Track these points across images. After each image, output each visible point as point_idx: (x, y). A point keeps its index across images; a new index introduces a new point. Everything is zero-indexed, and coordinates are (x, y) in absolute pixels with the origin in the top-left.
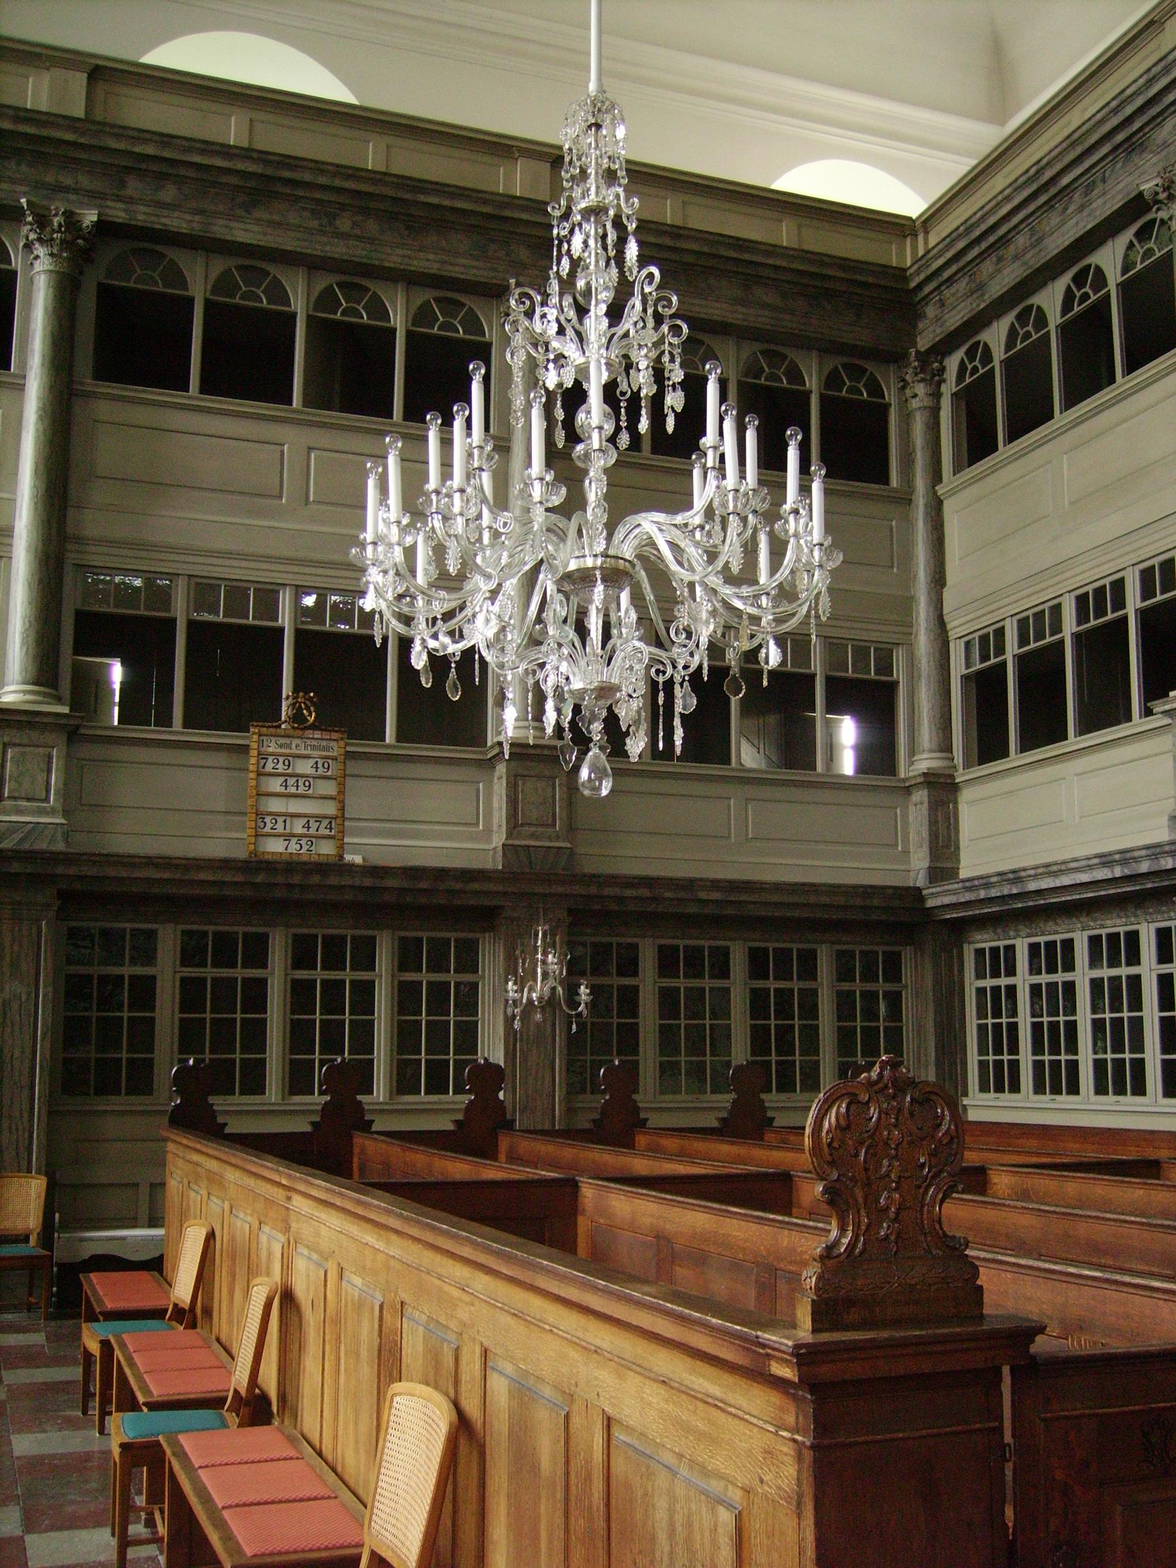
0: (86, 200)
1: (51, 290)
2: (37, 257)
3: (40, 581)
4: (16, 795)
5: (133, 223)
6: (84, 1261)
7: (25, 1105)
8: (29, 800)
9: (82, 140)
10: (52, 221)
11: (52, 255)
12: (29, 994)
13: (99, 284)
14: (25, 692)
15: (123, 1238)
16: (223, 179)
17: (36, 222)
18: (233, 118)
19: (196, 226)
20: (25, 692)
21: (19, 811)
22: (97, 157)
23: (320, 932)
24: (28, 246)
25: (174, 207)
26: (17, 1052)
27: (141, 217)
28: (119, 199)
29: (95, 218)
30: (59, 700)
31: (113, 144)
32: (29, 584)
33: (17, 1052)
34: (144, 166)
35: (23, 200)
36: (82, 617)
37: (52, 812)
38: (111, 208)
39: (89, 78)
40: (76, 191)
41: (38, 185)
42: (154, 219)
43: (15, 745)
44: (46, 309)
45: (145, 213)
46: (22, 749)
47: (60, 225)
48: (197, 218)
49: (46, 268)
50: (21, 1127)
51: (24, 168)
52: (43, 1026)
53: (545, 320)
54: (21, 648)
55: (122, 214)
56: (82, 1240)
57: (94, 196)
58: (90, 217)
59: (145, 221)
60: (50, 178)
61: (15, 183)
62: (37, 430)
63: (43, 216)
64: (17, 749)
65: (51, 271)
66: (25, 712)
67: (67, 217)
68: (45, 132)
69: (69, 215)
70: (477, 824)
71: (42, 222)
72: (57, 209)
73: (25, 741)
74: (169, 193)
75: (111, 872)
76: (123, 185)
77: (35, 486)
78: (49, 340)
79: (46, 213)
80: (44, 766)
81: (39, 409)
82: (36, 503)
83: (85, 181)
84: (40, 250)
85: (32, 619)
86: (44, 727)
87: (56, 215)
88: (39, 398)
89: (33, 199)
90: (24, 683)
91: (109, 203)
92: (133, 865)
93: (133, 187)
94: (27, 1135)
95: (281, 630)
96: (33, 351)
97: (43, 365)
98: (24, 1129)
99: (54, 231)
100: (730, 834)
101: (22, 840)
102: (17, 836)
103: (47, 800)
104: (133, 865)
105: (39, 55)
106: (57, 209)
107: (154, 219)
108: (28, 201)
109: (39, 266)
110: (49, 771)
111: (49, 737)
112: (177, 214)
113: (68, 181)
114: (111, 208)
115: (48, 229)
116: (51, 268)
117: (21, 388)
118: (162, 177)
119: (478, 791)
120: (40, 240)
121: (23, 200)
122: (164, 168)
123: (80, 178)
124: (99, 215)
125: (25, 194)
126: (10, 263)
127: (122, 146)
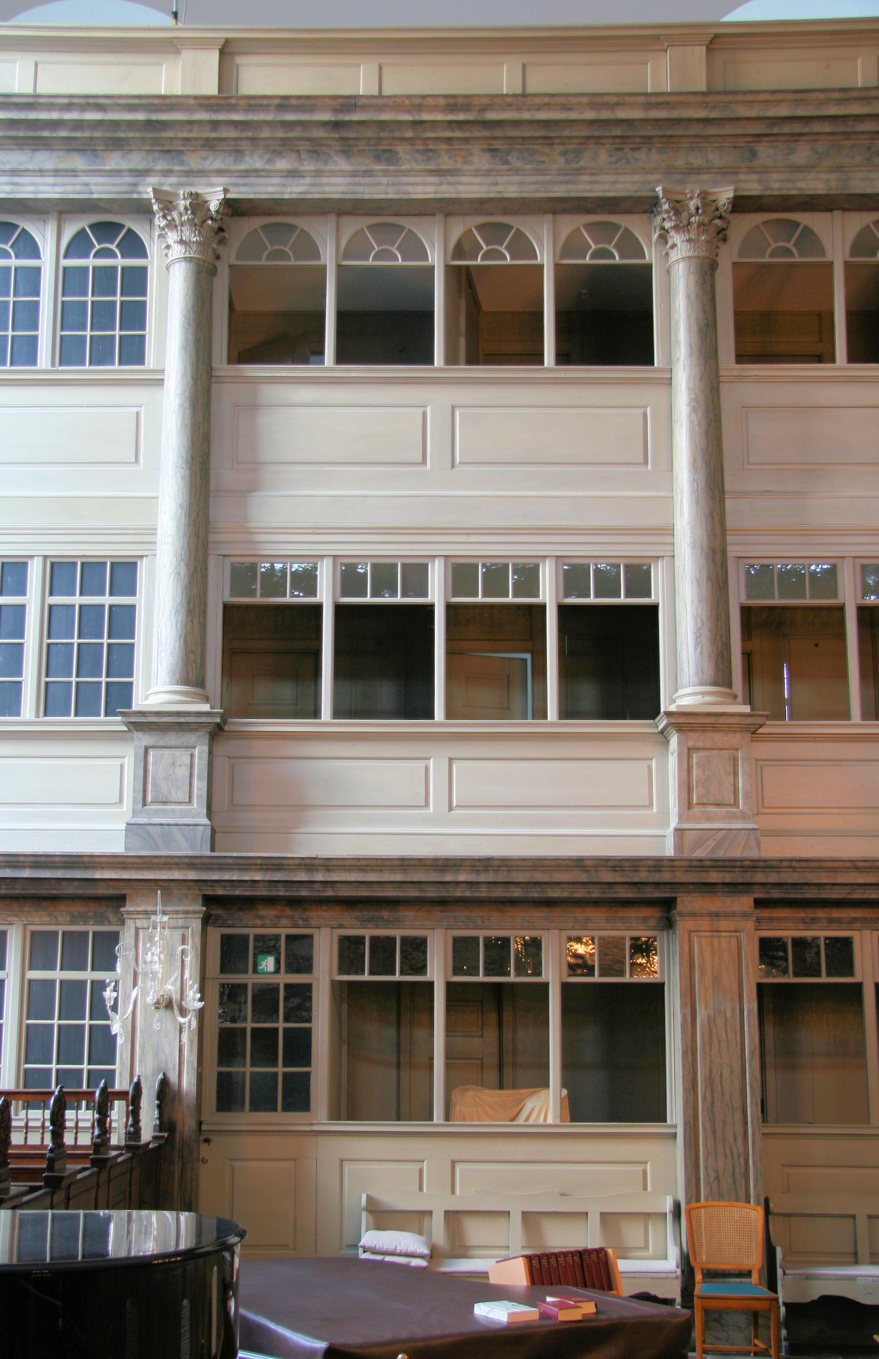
0: (719, 177)
1: (692, 277)
2: (673, 246)
3: (709, 578)
4: (705, 801)
5: (768, 193)
6: (813, 1302)
7: (739, 1128)
8: (717, 805)
9: (713, 115)
10: (687, 205)
11: (689, 241)
12: (733, 1009)
13: (735, 264)
14: (703, 694)
15: (852, 1278)
16: (861, 127)
17: (673, 208)
18: (859, 61)
19: (833, 184)
20: (703, 694)
21: (709, 818)
22: (728, 130)
23: (481, 934)
24: (663, 237)
25: (809, 168)
26: (726, 1072)
27: (777, 185)
28: (752, 170)
29: (731, 195)
30: (207, 699)
31: (743, 112)
32: (698, 582)
33: (726, 1072)
34: (776, 130)
35: (659, 189)
36: (746, 612)
37: (744, 817)
38: (744, 181)
39: (709, 50)
40: (708, 170)
41: (670, 171)
42: (789, 185)
43: (698, 749)
44: (688, 297)
45: (780, 181)
46: (707, 753)
47: (697, 209)
48: (834, 176)
49: (684, 255)
50: (735, 1151)
51: (654, 156)
52: (750, 1044)
53: (166, 251)
54: (695, 649)
55: (756, 186)
56: (808, 1277)
57: (726, 172)
58: (725, 195)
59: (779, 189)
60: (680, 162)
61: (647, 173)
62: (691, 422)
63: (678, 202)
64: (701, 754)
65: (690, 257)
66: (709, 714)
67: (703, 199)
68: (675, 114)
69: (703, 195)
70: (651, 805)
71: (678, 208)
72: (692, 192)
73: (709, 745)
74: (802, 154)
75: (812, 878)
76: (754, 154)
77: (694, 480)
78: (695, 328)
79: (678, 197)
80: (730, 769)
81: (691, 400)
82: (697, 498)
83: (715, 158)
84: (677, 238)
85: (705, 617)
86: (727, 729)
87: (691, 198)
88: (689, 389)
89: (667, 186)
90: (701, 684)
91: (742, 177)
92: (834, 870)
93: (766, 153)
94: (742, 1162)
95: (542, 608)
96: (678, 342)
97: (691, 355)
98: (739, 1155)
99: (691, 216)
100: (766, 808)
101: (714, 849)
102: (711, 844)
103: (736, 804)
104: (834, 870)
105: (657, 38)
106: (692, 192)
107: (789, 185)
108: (664, 190)
109: (675, 255)
110: (735, 774)
111: (190, 738)
112: (812, 175)
113: (697, 160)
114: (744, 181)
115: (685, 214)
116: (690, 254)
117: (669, 382)
118: (796, 137)
119: (650, 769)
120: (676, 228)
121: (659, 189)
122: (797, 128)
123: (711, 156)
124: (735, 191)
125: (658, 183)
126: (644, 257)
127: (754, 112)
